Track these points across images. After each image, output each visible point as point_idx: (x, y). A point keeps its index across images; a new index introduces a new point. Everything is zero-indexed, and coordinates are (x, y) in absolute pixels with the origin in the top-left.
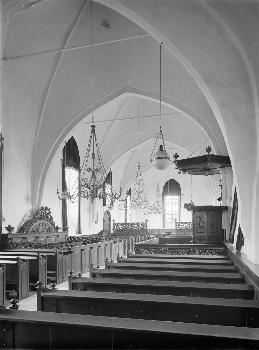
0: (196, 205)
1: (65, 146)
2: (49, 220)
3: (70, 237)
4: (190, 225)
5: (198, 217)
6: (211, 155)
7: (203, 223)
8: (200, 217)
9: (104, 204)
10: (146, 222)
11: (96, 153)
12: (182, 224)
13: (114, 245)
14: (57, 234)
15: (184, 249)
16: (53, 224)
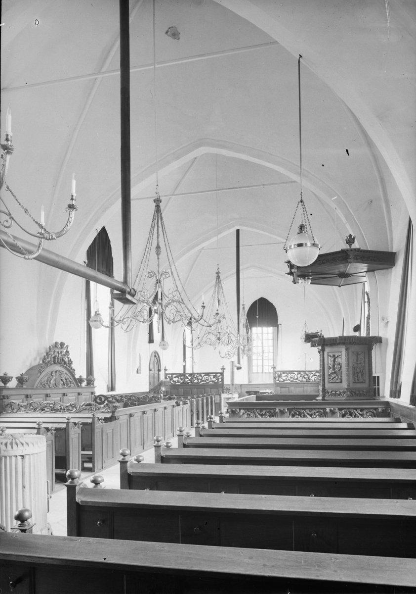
0: (325, 336)
1: (95, 239)
2: (67, 365)
3: (98, 396)
4: (299, 375)
5: (330, 356)
6: (356, 250)
7: (339, 366)
8: (334, 356)
9: (151, 341)
10: (222, 371)
11: (162, 245)
12: (285, 375)
13: (177, 408)
14: (79, 390)
15: (315, 409)
16: (72, 372)
